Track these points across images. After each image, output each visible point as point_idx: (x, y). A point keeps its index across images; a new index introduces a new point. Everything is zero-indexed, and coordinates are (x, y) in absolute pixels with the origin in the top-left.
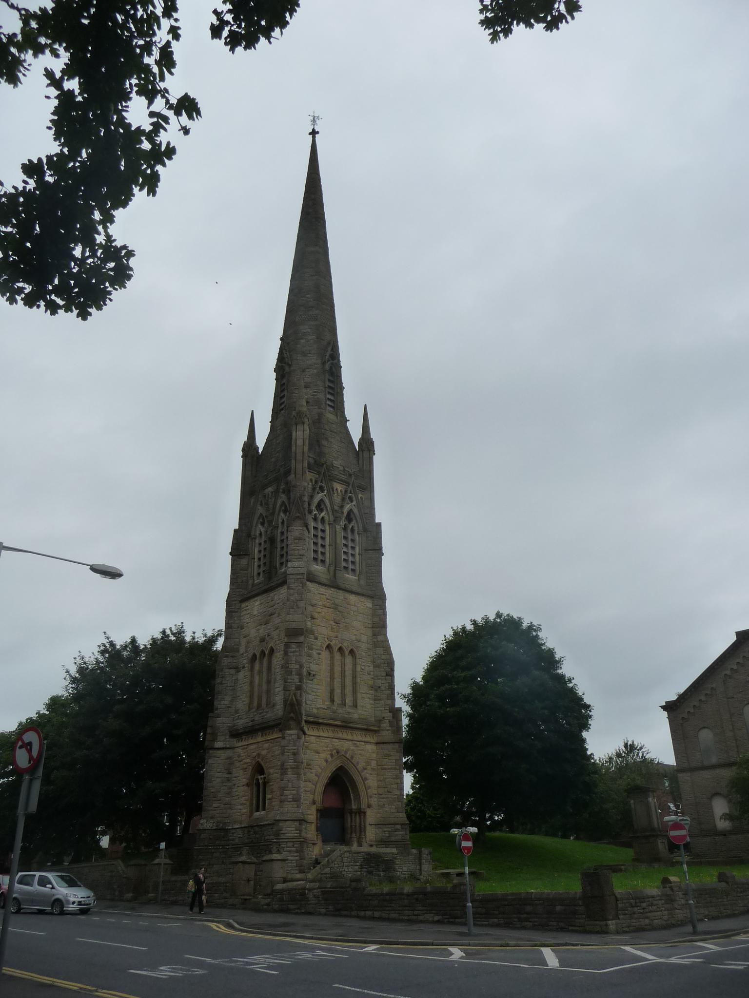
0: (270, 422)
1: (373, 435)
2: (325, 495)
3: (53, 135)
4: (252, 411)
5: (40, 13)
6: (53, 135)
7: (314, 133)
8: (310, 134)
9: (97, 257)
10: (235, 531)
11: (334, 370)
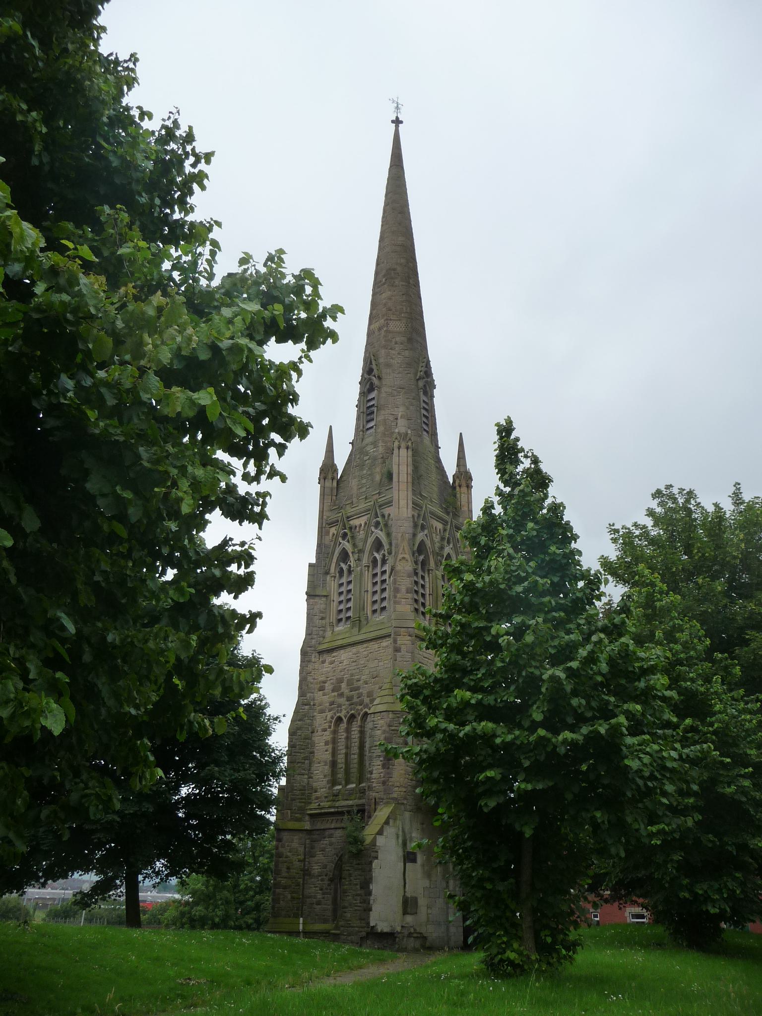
0: (352, 443)
1: (471, 465)
2: (426, 535)
3: (250, 611)
4: (331, 427)
5: (216, 601)
6: (250, 611)
7: (397, 122)
8: (393, 122)
9: (210, 838)
10: (311, 565)
11: (428, 389)
